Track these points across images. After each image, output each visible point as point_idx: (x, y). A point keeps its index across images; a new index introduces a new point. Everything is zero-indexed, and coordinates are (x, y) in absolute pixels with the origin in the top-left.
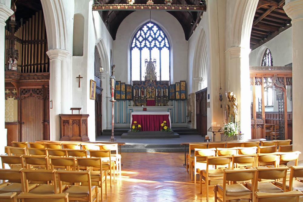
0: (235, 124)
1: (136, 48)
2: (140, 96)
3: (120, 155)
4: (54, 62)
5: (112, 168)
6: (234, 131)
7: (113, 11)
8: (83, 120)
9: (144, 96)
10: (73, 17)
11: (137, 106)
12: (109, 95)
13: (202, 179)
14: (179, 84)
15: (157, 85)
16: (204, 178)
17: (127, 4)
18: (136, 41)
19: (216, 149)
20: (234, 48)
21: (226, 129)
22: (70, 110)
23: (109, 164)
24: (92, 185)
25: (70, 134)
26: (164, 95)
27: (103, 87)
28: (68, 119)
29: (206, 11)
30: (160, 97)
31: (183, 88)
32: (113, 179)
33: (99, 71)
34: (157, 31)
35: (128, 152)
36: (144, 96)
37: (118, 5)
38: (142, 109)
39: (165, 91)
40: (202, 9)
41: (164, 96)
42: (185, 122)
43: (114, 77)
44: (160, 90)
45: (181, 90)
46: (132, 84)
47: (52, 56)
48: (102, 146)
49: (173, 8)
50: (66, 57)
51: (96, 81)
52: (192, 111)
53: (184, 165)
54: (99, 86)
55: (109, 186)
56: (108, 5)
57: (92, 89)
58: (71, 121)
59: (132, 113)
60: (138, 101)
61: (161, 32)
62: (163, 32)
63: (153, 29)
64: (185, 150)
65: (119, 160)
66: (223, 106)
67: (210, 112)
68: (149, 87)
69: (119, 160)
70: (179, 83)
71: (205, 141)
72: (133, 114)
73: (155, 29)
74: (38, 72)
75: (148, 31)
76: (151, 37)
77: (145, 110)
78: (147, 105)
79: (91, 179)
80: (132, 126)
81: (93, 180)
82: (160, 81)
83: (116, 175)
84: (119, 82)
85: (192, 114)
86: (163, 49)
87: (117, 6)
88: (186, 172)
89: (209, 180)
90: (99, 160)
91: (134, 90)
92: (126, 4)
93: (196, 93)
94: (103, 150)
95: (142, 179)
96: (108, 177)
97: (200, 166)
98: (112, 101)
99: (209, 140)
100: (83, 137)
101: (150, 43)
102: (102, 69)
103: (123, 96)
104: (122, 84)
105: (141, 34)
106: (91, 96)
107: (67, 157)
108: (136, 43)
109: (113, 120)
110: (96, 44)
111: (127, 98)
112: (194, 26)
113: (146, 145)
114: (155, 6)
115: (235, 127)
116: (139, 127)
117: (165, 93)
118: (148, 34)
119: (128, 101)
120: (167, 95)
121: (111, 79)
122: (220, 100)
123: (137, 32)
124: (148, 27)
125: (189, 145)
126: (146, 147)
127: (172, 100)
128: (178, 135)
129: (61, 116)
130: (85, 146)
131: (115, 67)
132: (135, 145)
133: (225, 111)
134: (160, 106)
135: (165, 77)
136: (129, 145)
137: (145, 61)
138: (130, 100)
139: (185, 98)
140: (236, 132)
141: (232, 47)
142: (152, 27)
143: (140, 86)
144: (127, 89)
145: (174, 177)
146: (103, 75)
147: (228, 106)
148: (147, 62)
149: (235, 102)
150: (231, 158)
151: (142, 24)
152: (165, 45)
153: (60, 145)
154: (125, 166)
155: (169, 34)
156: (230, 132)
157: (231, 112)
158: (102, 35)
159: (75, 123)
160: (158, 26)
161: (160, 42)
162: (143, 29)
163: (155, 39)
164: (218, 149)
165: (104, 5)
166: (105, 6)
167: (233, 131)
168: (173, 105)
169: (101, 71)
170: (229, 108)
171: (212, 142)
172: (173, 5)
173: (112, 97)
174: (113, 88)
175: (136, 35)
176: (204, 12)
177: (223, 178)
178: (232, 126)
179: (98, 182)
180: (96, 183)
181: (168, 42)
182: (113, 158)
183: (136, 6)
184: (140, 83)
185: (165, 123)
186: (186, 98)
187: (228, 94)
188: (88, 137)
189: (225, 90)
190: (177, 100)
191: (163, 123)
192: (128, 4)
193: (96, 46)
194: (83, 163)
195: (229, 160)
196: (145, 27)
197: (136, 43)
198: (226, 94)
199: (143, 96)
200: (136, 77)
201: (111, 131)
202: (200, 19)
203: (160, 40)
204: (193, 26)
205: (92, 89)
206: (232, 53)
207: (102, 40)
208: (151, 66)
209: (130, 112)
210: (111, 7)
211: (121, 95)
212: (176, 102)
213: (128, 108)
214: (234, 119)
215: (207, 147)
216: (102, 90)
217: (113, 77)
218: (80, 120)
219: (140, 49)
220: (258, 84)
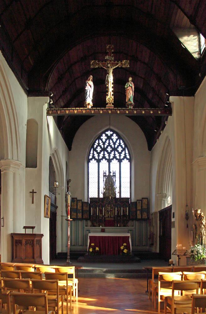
0: (203, 246)
2: (98, 215)
3: (77, 280)
4: (5, 174)
5: (69, 294)
6: (202, 254)
7: (69, 116)
8: (37, 241)
9: (102, 215)
10: (26, 122)
11: (94, 226)
12: (65, 214)
13: (167, 307)
14: (140, 201)
15: (116, 202)
16: (170, 306)
17: (85, 108)
18: (93, 152)
19: (182, 272)
20: (202, 158)
21: (192, 252)
22: (23, 228)
23: (66, 288)
24: (49, 310)
25: (23, 255)
26: (124, 214)
27: (58, 204)
28: (21, 239)
29: (171, 115)
30: (120, 216)
31: (145, 207)
32: (70, 306)
33: (54, 186)
35: (85, 277)
36: (103, 216)
37: (74, 108)
39: (125, 210)
40: (168, 113)
41: (124, 215)
44: (119, 209)
47: (4, 167)
48: (58, 269)
49: (135, 112)
50: (18, 169)
51: (50, 197)
52: (155, 233)
53: (146, 292)
54: (53, 203)
55: (188, 39)
56: (64, 109)
57: (46, 205)
58: (24, 242)
59: (89, 234)
60: (96, 221)
61: (121, 141)
62: (123, 142)
63: (112, 137)
64: (147, 275)
65: (76, 286)
66: (189, 226)
67: (175, 233)
68: (108, 205)
69: (76, 286)
70: (140, 200)
71: (170, 265)
72: (90, 235)
73: (115, 137)
77: (103, 231)
78: (106, 226)
79: (48, 304)
80: (89, 248)
81: (50, 305)
83: (73, 301)
85: (155, 236)
86: (123, 161)
87: (73, 110)
88: (148, 299)
89: (174, 307)
90: (56, 283)
91: (92, 208)
92: (83, 108)
93: (159, 211)
94: (58, 273)
95: (132, 244)
96: (65, 304)
97: (164, 292)
98: (68, 220)
99: (173, 265)
100: (37, 260)
101: (109, 154)
102: (57, 184)
103: (80, 216)
104: (78, 202)
105: (99, 143)
106: (45, 213)
107: (21, 278)
108: (93, 154)
109: (69, 242)
110: (50, 155)
111: (84, 218)
112: (158, 134)
113: (105, 269)
114: (115, 110)
115: (203, 250)
116: (96, 250)
117: (125, 211)
118: (107, 144)
119: (85, 220)
120: (127, 215)
121: (66, 195)
122: (186, 218)
123: (95, 142)
124: (107, 135)
125: (152, 268)
126: (105, 272)
127: (133, 220)
128: (139, 259)
129: (13, 236)
130: (40, 268)
131: (71, 182)
132: (93, 270)
133: (192, 232)
134: (120, 226)
135: (126, 193)
136: (86, 270)
137: (104, 176)
138: (86, 220)
139: (147, 218)
140: (204, 255)
141: (199, 157)
142: (112, 135)
143: (99, 204)
144: (84, 207)
145: (135, 305)
146: (58, 191)
147: (195, 225)
149: (203, 221)
150: (199, 283)
151: (100, 132)
152: (125, 157)
153: (13, 267)
154: (82, 292)
155: (129, 143)
156: (197, 255)
157: (198, 232)
158: (57, 143)
159: (28, 243)
160: (118, 135)
161: (120, 153)
162: (102, 137)
163: (115, 149)
164: (185, 273)
165: (60, 109)
166: (61, 110)
167: (200, 254)
168: (134, 226)
169: (55, 186)
170: (196, 228)
171: (176, 266)
172: (136, 109)
173: (67, 215)
174: (69, 205)
175: (94, 144)
176: (169, 117)
177: (191, 306)
178: (200, 248)
179: (54, 307)
180: (52, 308)
181: (129, 153)
182: (70, 283)
183: (94, 110)
185: (125, 246)
186: (148, 218)
187: (195, 211)
188: (42, 259)
189: (191, 207)
190: (137, 219)
191: (123, 245)
192: (85, 107)
193: (50, 158)
194: (38, 286)
195: (197, 285)
196: (104, 135)
197: (93, 154)
198: (193, 211)
200: (93, 193)
201: (66, 254)
202: (165, 125)
204: (157, 134)
205: (46, 205)
206: (200, 164)
207: (57, 150)
208: (109, 180)
209: (87, 233)
210: (67, 112)
211: (77, 214)
212: (137, 222)
213: (85, 229)
214: (202, 240)
215: (172, 271)
216: (56, 207)
217: (69, 193)
218: (33, 241)
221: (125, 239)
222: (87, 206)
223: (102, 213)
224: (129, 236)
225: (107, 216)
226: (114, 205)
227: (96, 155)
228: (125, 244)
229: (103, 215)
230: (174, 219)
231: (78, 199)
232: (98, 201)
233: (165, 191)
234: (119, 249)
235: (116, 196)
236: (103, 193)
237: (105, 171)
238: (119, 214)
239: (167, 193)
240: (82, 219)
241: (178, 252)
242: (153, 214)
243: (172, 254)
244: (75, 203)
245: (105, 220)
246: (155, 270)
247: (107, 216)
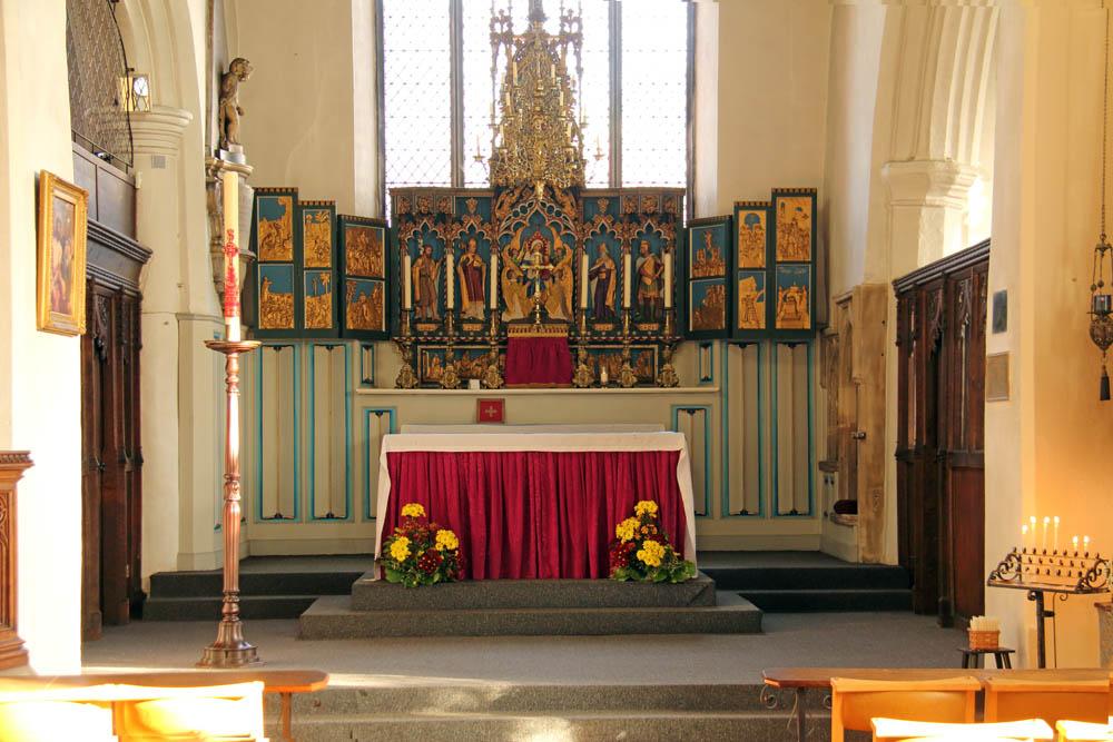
2: (451, 305)
9: (481, 306)
11: (426, 383)
12: (205, 302)
14: (762, 215)
15: (584, 219)
19: (1053, 726)
27: (156, 230)
31: (792, 247)
36: (488, 311)
39: (649, 270)
41: (646, 309)
42: (810, 513)
43: (242, 160)
44: (609, 265)
45: (780, 259)
48: (133, 703)
51: (89, 186)
52: (867, 426)
54: (114, 224)
57: (53, 248)
71: (971, 660)
77: (491, 413)
78: (509, 378)
82: (615, 196)
84: (286, 201)
85: (866, 451)
93: (896, 283)
98: (227, 349)
99: (1002, 657)
102: (141, 86)
103: (320, 311)
104: (307, 216)
109: (236, 497)
111: (350, 326)
113: (497, 687)
116: (439, 547)
117: (648, 281)
120: (668, 304)
125: (829, 688)
127: (704, 338)
134: (612, 383)
136: (364, 692)
137: (494, 36)
138: (369, 337)
143: (457, 230)
146: (149, 139)
168: (717, 378)
173: (225, 311)
185: (645, 518)
186: (819, 326)
190: (731, 334)
191: (634, 514)
199: (475, 310)
201: (213, 581)
205: (53, 248)
212: (734, 353)
213: (359, 404)
216: (140, 257)
221: (653, 472)
222: (370, 249)
223: (479, 294)
224: (677, 453)
225: (516, 311)
226: (567, 238)
228: (647, 507)
229: (493, 305)
230: (1001, 337)
231: (302, 197)
232: (454, 212)
233: (948, 143)
234: (607, 541)
235: (588, 173)
236: (488, 154)
237: (504, 7)
238: (609, 302)
239: (961, 158)
240: (340, 336)
241: (1033, 569)
242: (850, 299)
243: (989, 585)
244: (280, 223)
245: (504, 342)
246: (847, 695)
247: (516, 311)
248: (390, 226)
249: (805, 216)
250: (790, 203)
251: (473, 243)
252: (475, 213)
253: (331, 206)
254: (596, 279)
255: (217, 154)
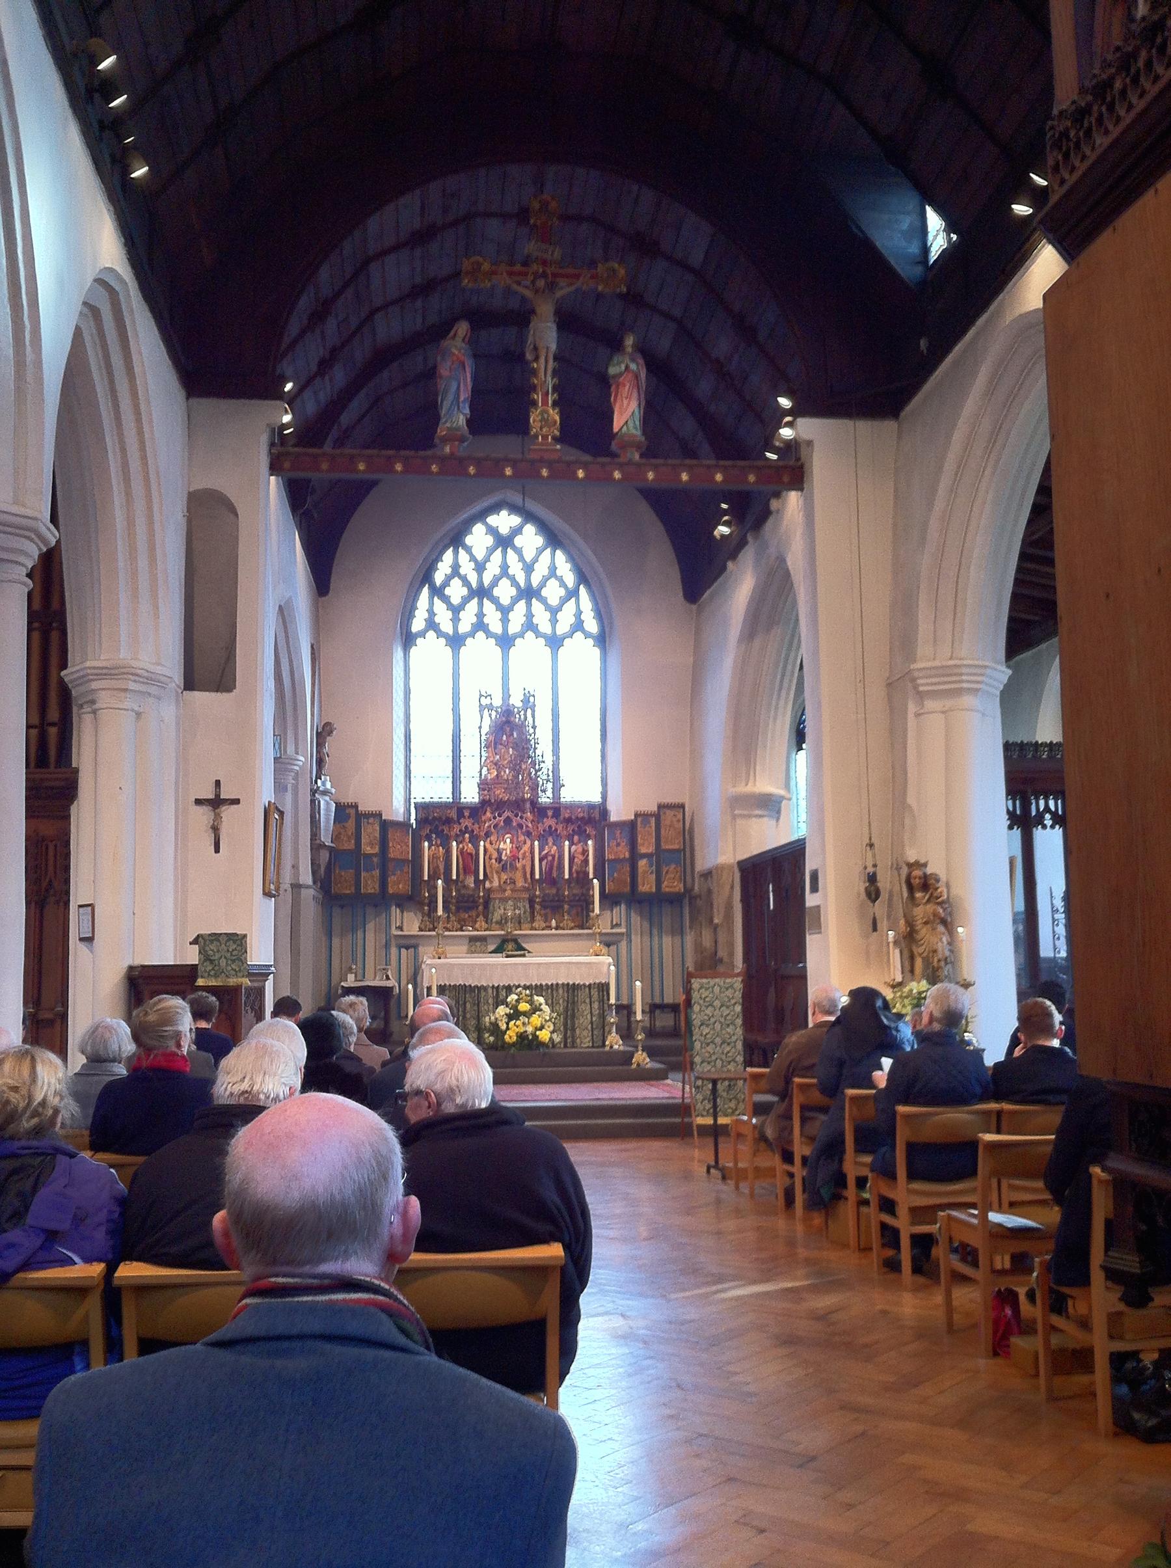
1: (431, 634)
14: (653, 820)
18: (431, 603)
34: (540, 551)
36: (477, 881)
38: (504, 955)
43: (328, 785)
46: (413, 821)
63: (518, 541)
70: (651, 815)
74: (248, 989)
75: (491, 551)
76: (460, 583)
82: (557, 809)
84: (353, 811)
93: (740, 863)
104: (364, 821)
105: (456, 567)
108: (431, 612)
118: (493, 569)
124: (492, 531)
142: (517, 531)
143: (456, 829)
148: (490, 707)
152: (578, 626)
160: (544, 528)
163: (529, 593)
184: (453, 814)
197: (431, 612)
203: (554, 601)
206: (921, 689)
219: (456, 641)
220: (1048, 822)
227: (443, 617)
229: (481, 877)
248: (414, 827)
249: (679, 821)
250: (669, 813)
251: (467, 835)
252: (469, 817)
253: (379, 815)
254: (545, 861)
255: (316, 782)
